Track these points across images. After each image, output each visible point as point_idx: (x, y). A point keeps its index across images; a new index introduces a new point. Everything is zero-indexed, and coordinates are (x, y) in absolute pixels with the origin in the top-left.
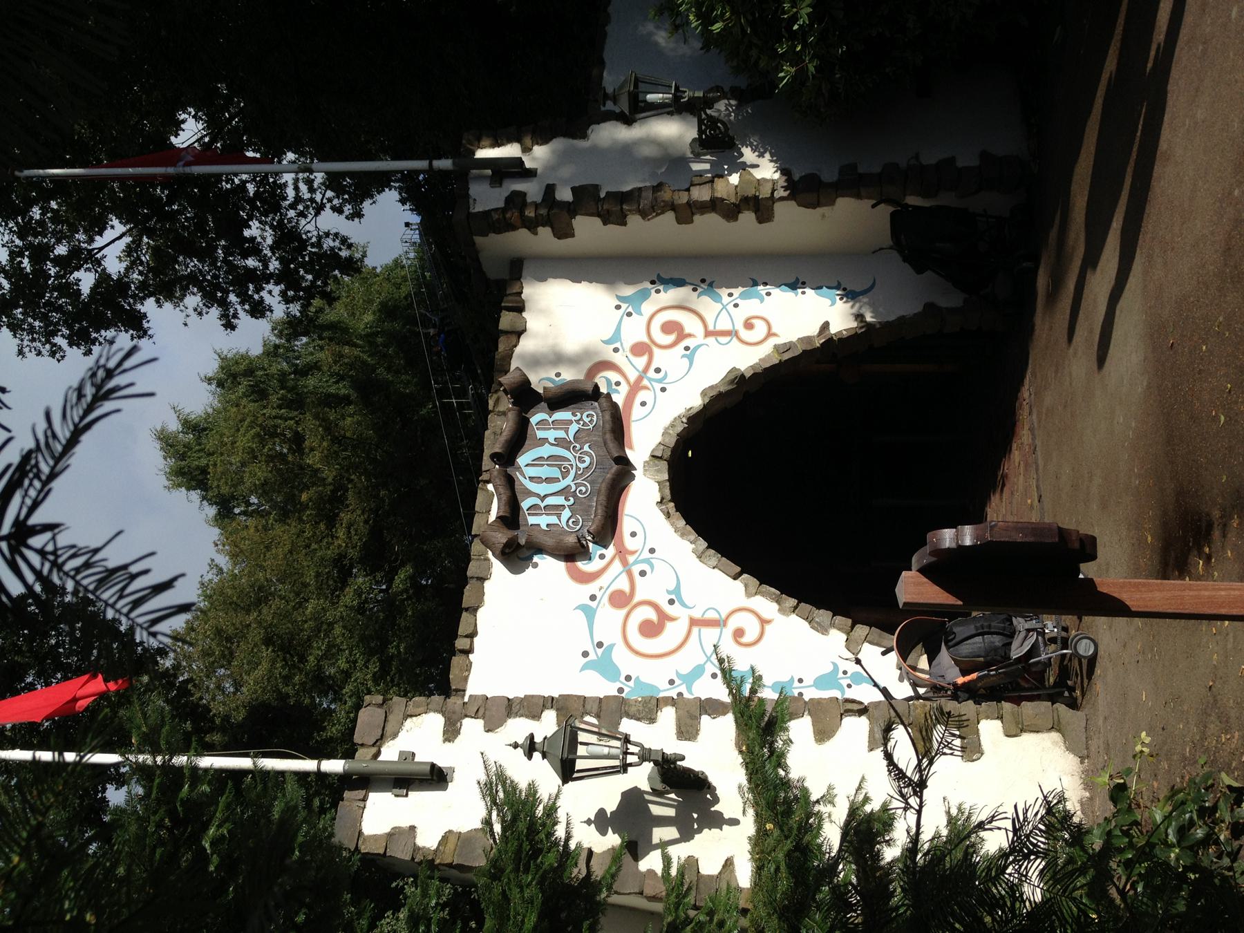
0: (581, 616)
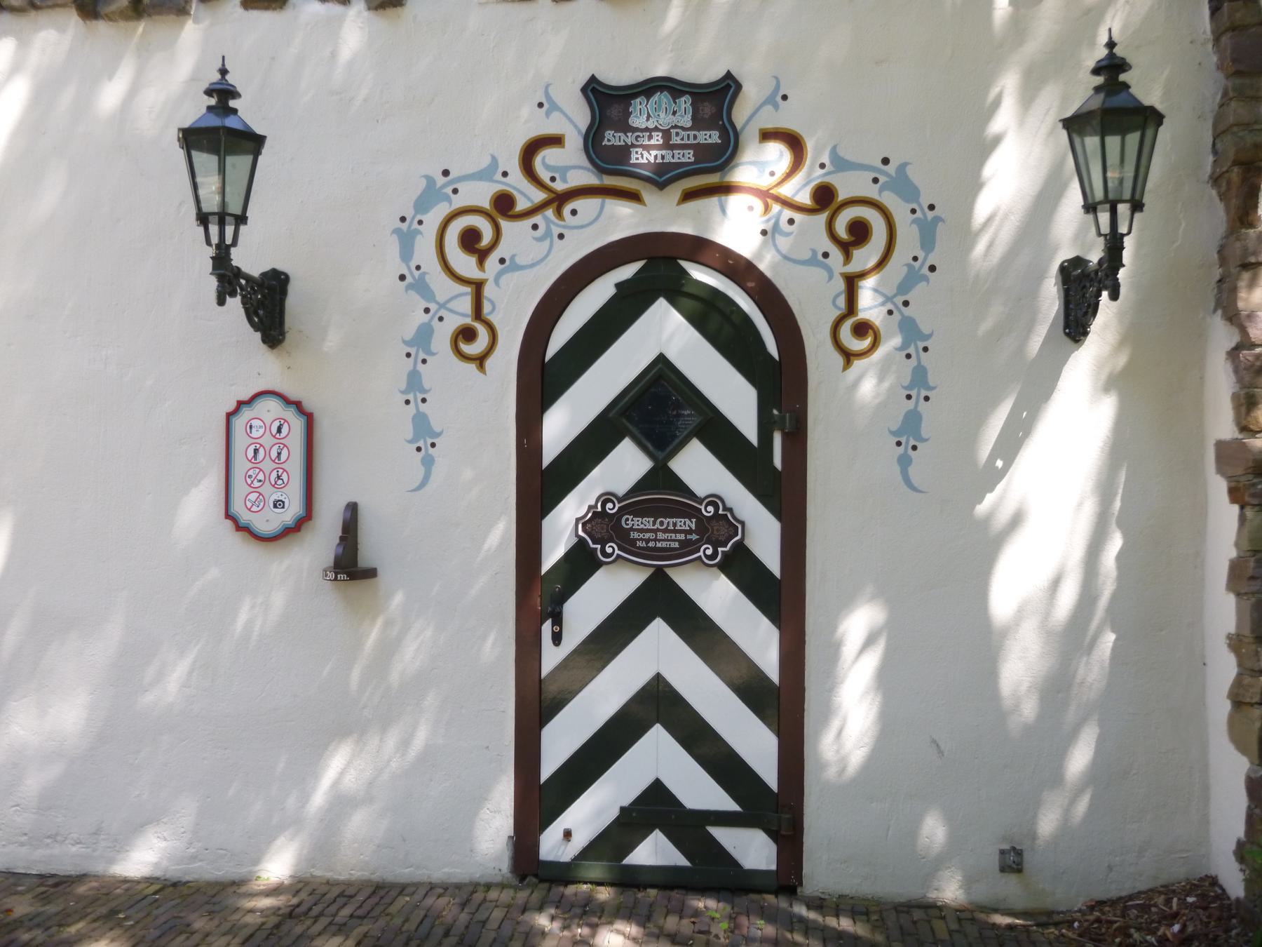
0: (486, 162)
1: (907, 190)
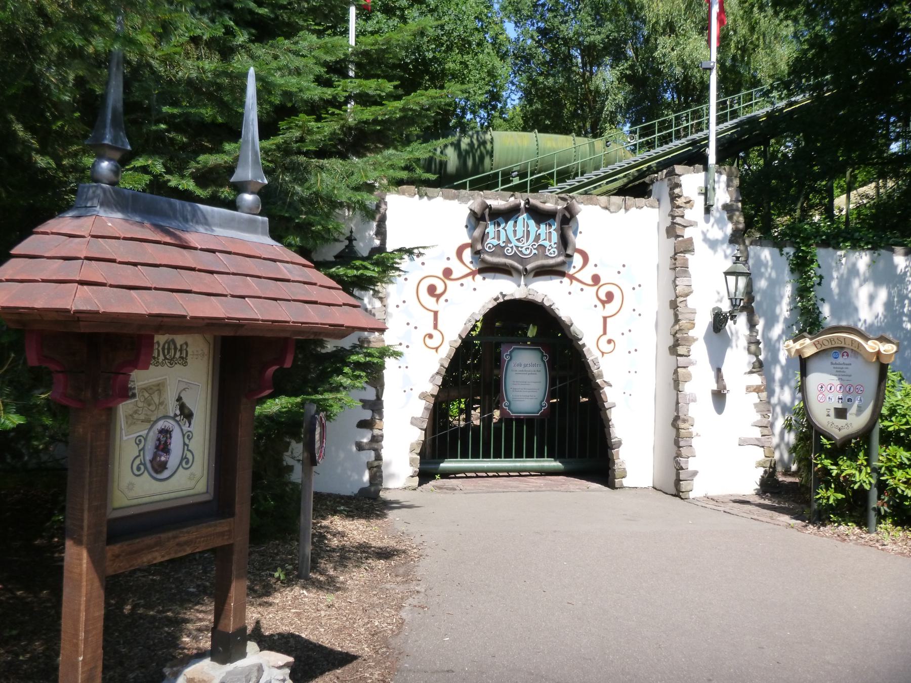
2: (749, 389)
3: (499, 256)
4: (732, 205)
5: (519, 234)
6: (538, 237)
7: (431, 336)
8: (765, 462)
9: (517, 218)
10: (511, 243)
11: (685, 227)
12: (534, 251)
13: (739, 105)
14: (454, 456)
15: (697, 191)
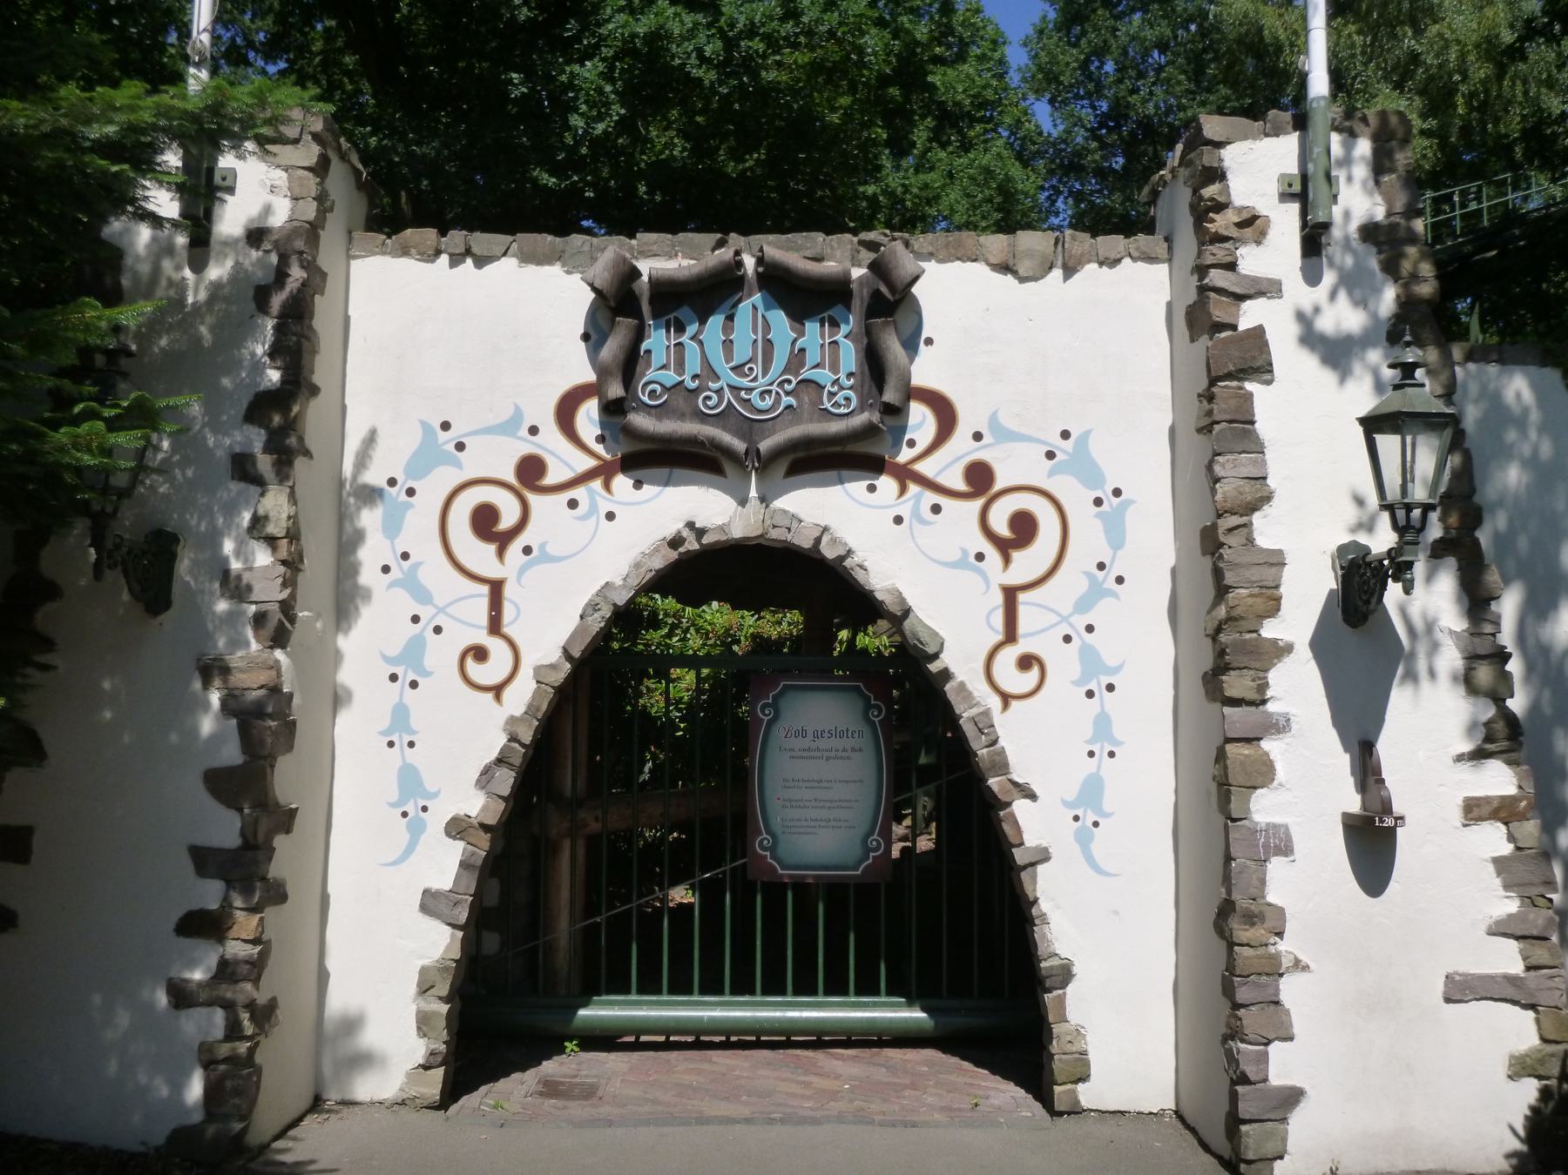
0: (506, 414)
1: (1088, 471)
2: (1475, 810)
3: (682, 416)
4: (1393, 227)
5: (742, 353)
6: (797, 358)
7: (480, 654)
8: (1541, 1061)
9: (735, 305)
10: (717, 378)
11: (1242, 298)
12: (787, 400)
13: (1480, 202)
14: (619, 985)
15: (1273, 189)
